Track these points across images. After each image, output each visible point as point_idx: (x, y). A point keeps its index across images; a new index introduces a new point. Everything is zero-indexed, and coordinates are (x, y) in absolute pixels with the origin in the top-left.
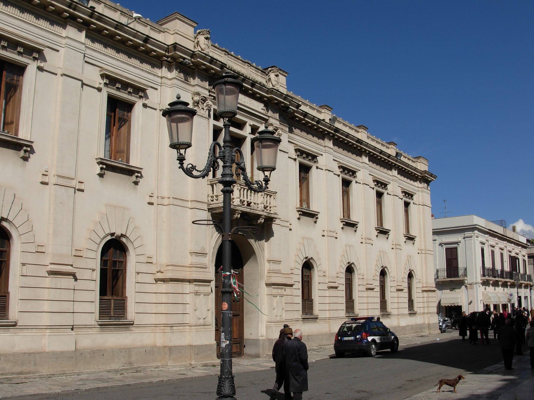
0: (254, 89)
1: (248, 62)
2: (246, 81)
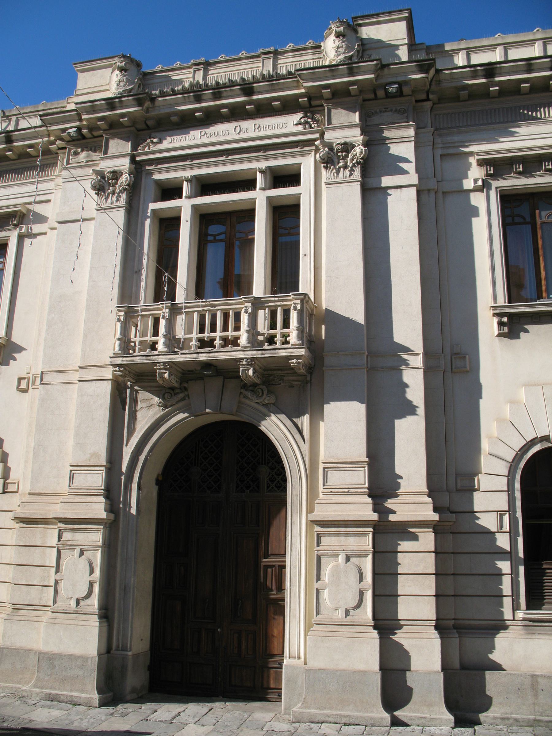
0: (255, 97)
1: (266, 50)
2: (224, 94)
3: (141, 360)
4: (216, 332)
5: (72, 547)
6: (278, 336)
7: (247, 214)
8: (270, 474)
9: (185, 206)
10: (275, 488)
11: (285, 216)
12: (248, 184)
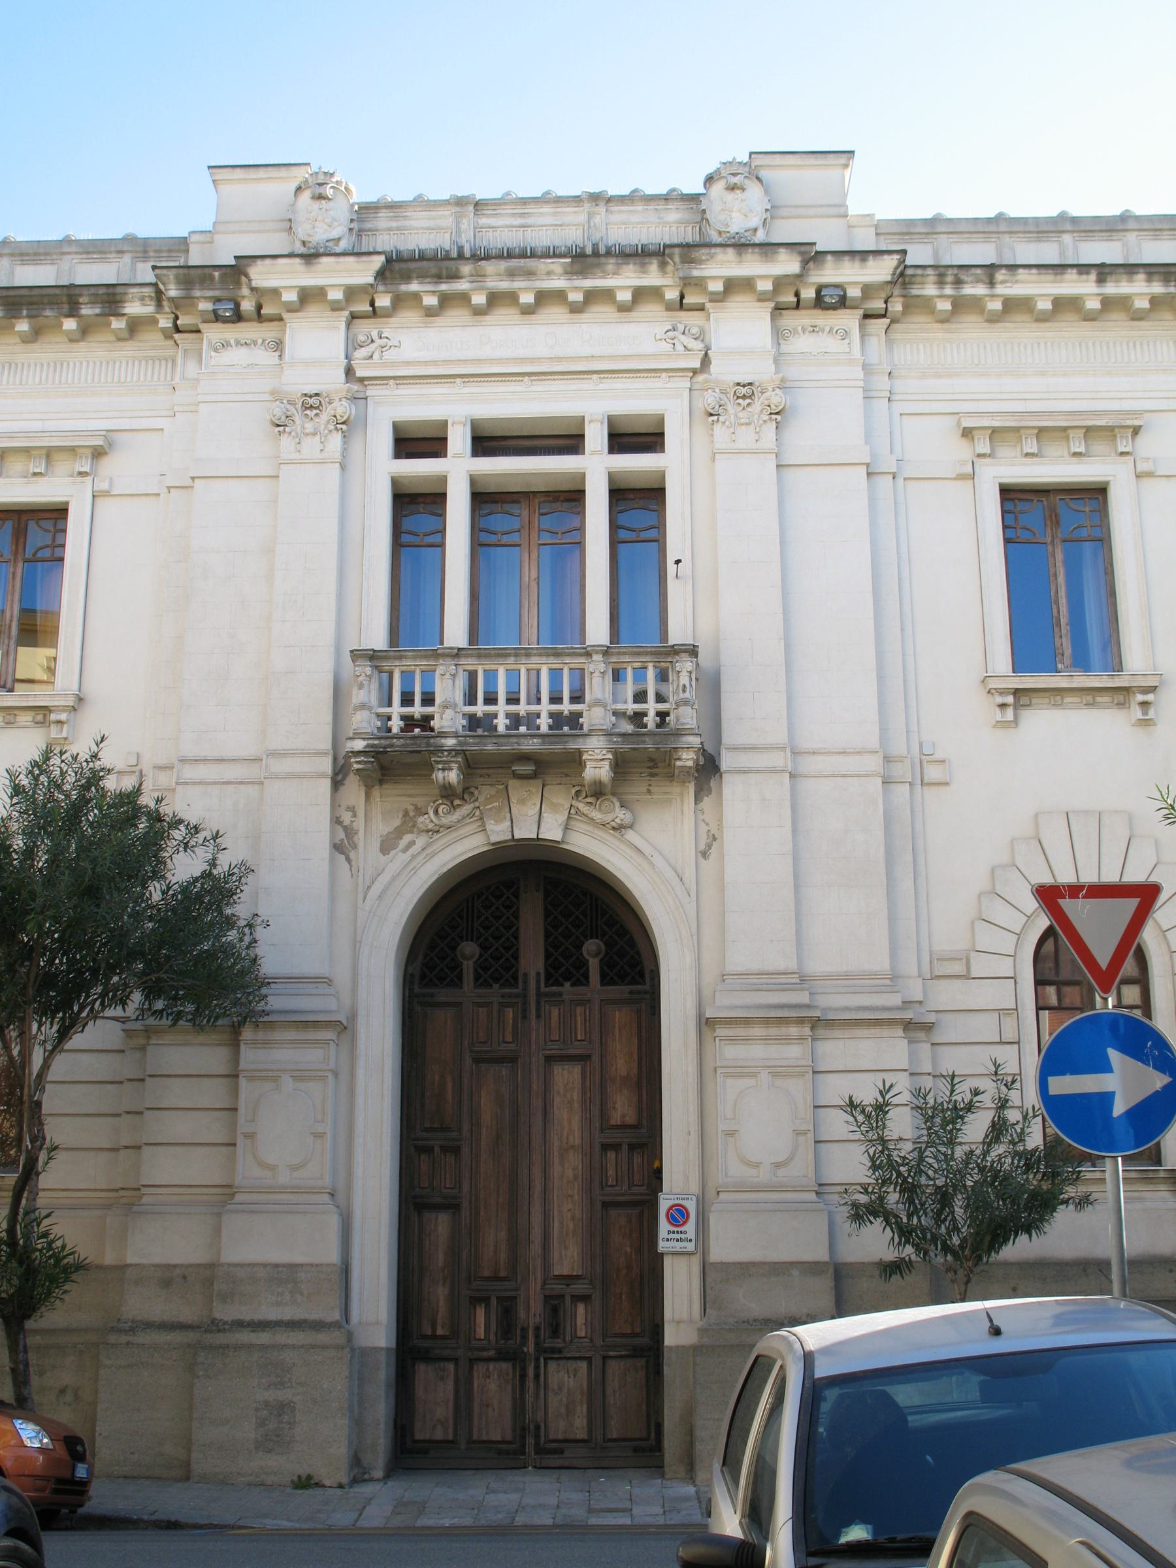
3: (407, 745)
4: (646, 702)
5: (753, 1070)
6: (544, 715)
7: (571, 497)
8: (481, 955)
9: (458, 470)
10: (616, 979)
11: (638, 502)
12: (569, 441)
